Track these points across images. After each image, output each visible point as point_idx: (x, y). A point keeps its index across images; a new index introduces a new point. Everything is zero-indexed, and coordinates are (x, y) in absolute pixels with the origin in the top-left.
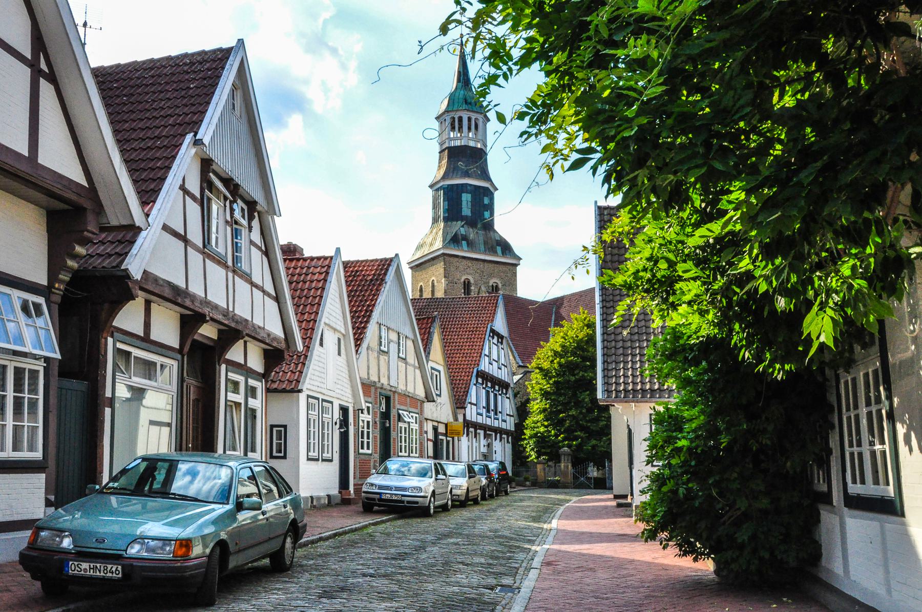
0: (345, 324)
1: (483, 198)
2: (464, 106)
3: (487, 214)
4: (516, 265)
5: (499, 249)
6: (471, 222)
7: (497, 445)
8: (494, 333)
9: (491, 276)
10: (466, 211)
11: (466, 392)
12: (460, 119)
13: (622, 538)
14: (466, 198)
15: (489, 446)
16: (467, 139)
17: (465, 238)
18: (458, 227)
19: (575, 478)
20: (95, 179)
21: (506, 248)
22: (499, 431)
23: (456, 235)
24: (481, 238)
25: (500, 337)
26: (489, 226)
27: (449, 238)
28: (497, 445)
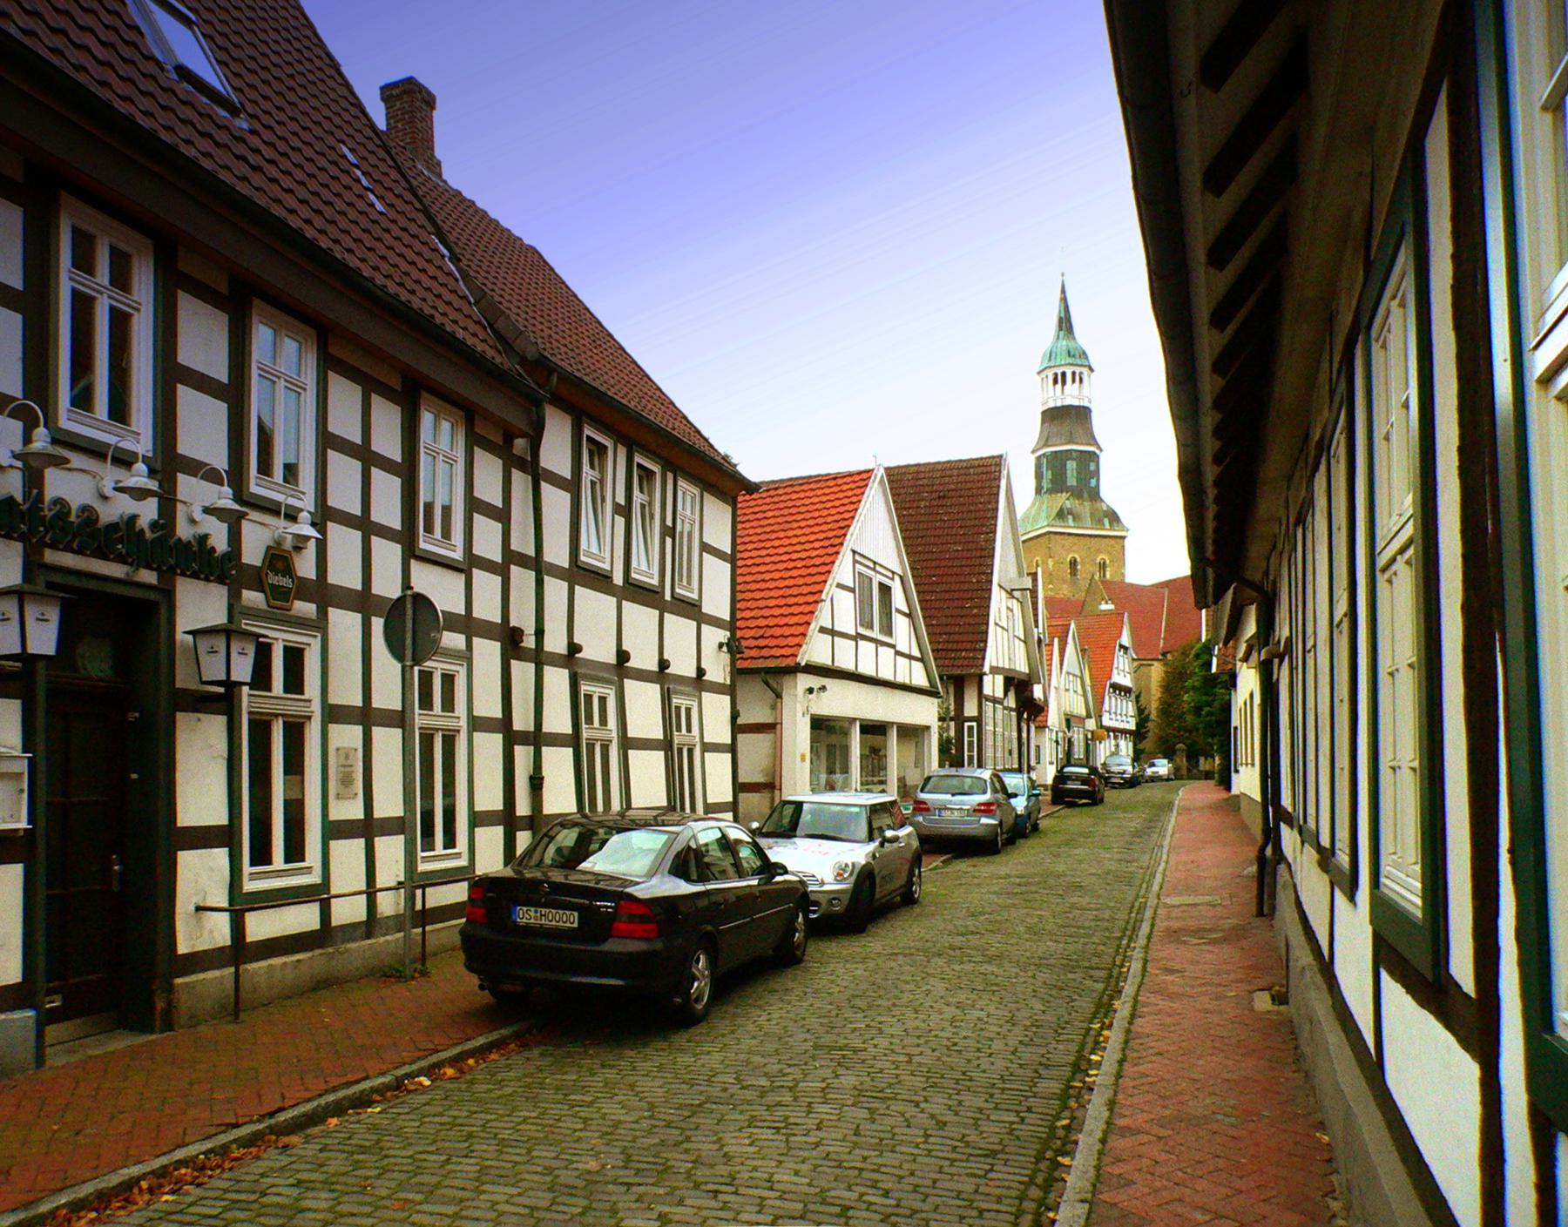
0: (902, 562)
1: (1089, 462)
2: (1070, 360)
3: (1093, 482)
4: (1123, 538)
5: (1106, 521)
6: (1077, 493)
7: (1122, 743)
8: (1121, 646)
9: (1099, 551)
10: (1072, 481)
11: (1102, 703)
12: (1064, 374)
13: (831, 1215)
14: (1071, 465)
15: (1117, 746)
16: (1070, 395)
17: (1070, 512)
18: (1062, 500)
19: (1189, 770)
20: (1328, 890)
21: (1114, 518)
22: (1124, 732)
23: (1061, 510)
24: (1087, 510)
25: (1126, 649)
26: (1095, 495)
27: (1055, 512)
28: (1122, 743)
